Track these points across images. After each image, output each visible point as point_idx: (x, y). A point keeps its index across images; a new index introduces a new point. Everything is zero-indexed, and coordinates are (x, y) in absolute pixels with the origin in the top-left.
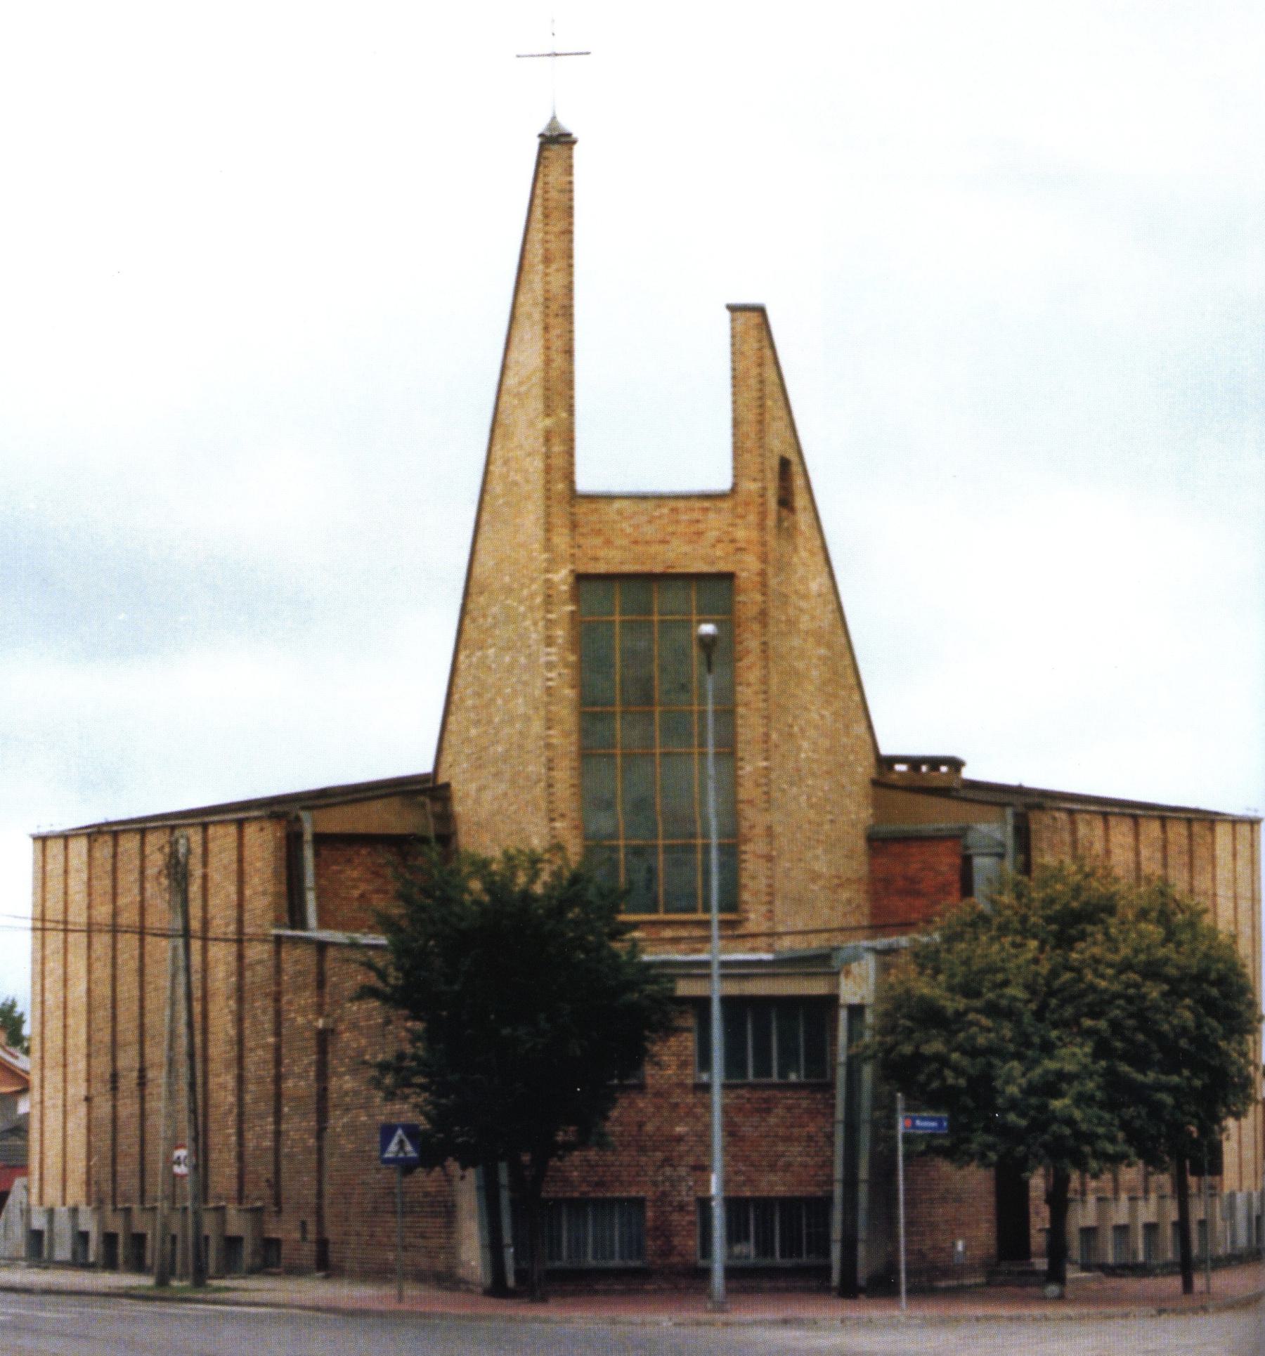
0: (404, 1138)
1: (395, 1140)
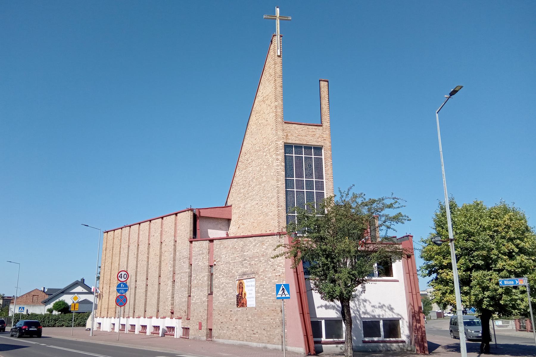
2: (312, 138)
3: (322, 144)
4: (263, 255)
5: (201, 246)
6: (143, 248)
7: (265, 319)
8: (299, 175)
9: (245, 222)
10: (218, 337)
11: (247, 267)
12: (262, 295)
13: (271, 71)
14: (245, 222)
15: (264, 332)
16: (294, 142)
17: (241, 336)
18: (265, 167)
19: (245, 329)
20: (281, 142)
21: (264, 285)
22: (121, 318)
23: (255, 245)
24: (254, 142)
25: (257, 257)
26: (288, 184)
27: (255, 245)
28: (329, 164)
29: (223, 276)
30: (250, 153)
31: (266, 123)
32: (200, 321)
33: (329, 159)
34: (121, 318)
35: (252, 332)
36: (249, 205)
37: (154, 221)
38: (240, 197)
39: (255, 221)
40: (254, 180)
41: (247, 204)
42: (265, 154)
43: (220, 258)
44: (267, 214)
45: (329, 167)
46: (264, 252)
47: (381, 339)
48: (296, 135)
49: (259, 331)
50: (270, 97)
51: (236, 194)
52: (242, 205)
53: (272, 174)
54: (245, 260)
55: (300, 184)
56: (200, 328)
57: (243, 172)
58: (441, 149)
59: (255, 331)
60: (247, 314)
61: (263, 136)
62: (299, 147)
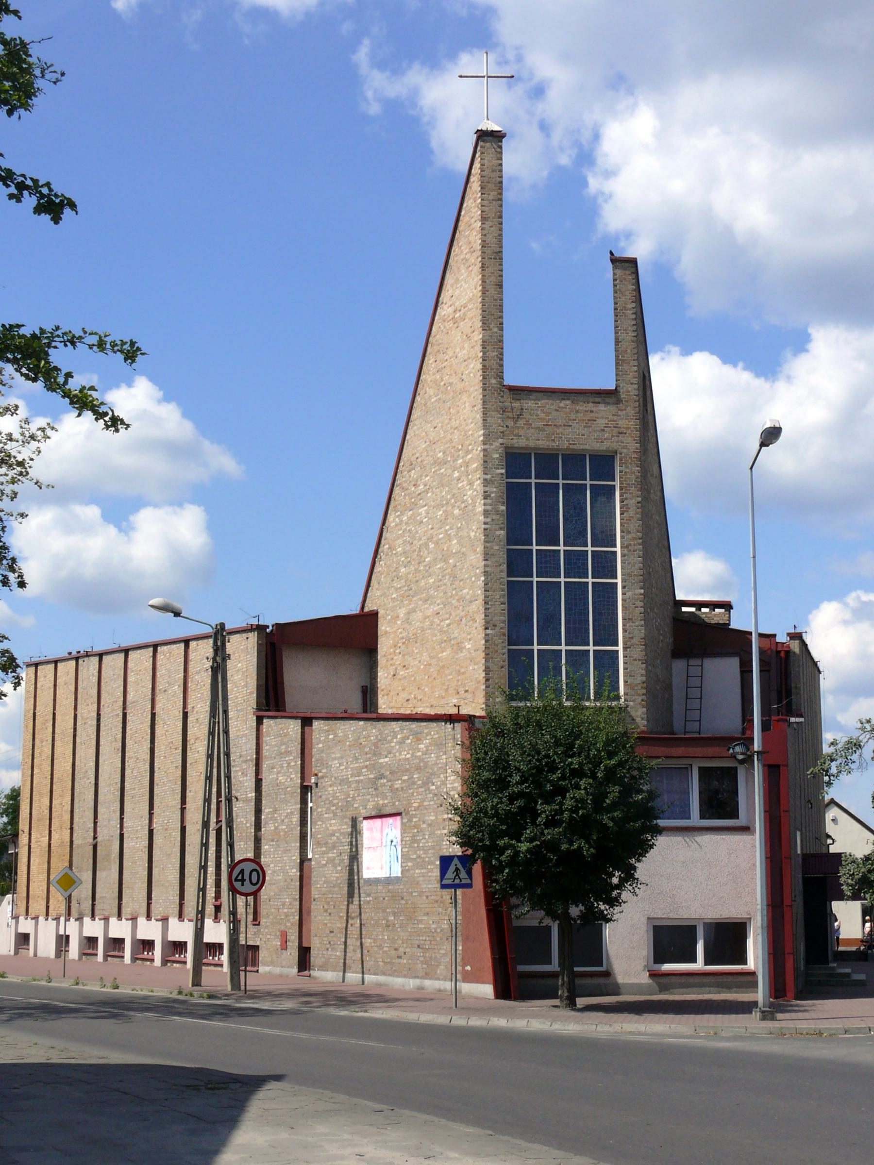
0: (460, 866)
1: (452, 868)
2: (585, 431)
3: (615, 446)
4: (418, 768)
5: (283, 732)
6: (138, 724)
7: (421, 921)
8: (549, 535)
9: (409, 660)
10: (323, 968)
11: (384, 797)
12: (417, 866)
13: (472, 239)
14: (409, 660)
15: (419, 953)
16: (531, 444)
17: (372, 963)
18: (456, 511)
19: (380, 947)
20: (496, 444)
21: (418, 842)
22: (87, 920)
23: (402, 742)
24: (432, 435)
25: (407, 770)
26: (517, 563)
27: (402, 742)
28: (632, 502)
29: (335, 814)
30: (423, 467)
31: (460, 386)
32: (283, 928)
33: (633, 489)
34: (87, 920)
35: (393, 952)
36: (420, 615)
37: (165, 648)
38: (397, 589)
39: (434, 662)
40: (432, 546)
41: (414, 611)
42: (456, 474)
43: (329, 767)
44: (459, 647)
45: (631, 513)
46: (421, 760)
47: (699, 965)
48: (540, 424)
49: (408, 950)
50: (470, 315)
51: (389, 580)
52: (402, 613)
53: (472, 534)
54: (382, 776)
55: (548, 563)
56: (284, 946)
57: (405, 518)
58: (564, 661)
59: (402, 950)
60: (384, 911)
61: (454, 423)
62: (547, 461)
